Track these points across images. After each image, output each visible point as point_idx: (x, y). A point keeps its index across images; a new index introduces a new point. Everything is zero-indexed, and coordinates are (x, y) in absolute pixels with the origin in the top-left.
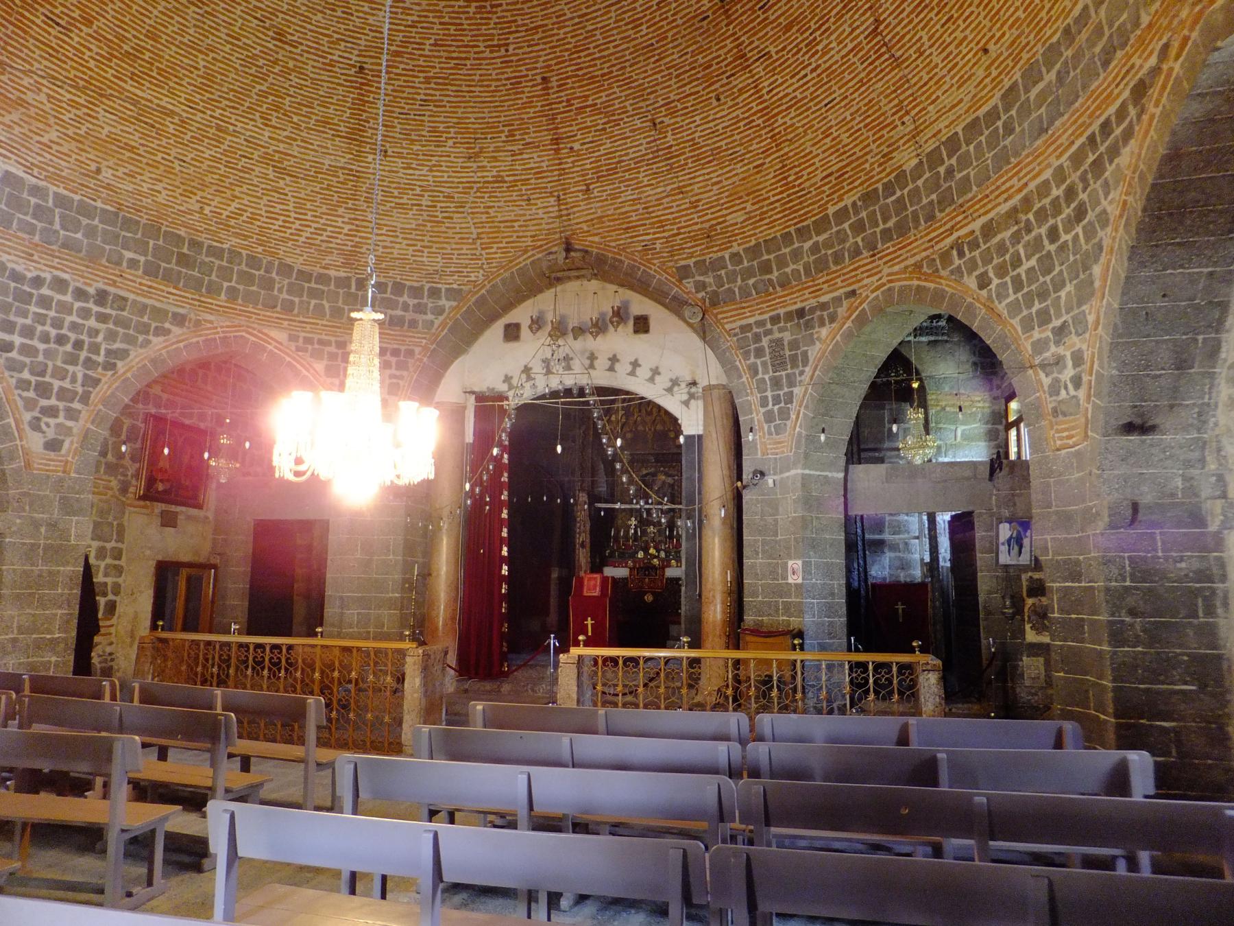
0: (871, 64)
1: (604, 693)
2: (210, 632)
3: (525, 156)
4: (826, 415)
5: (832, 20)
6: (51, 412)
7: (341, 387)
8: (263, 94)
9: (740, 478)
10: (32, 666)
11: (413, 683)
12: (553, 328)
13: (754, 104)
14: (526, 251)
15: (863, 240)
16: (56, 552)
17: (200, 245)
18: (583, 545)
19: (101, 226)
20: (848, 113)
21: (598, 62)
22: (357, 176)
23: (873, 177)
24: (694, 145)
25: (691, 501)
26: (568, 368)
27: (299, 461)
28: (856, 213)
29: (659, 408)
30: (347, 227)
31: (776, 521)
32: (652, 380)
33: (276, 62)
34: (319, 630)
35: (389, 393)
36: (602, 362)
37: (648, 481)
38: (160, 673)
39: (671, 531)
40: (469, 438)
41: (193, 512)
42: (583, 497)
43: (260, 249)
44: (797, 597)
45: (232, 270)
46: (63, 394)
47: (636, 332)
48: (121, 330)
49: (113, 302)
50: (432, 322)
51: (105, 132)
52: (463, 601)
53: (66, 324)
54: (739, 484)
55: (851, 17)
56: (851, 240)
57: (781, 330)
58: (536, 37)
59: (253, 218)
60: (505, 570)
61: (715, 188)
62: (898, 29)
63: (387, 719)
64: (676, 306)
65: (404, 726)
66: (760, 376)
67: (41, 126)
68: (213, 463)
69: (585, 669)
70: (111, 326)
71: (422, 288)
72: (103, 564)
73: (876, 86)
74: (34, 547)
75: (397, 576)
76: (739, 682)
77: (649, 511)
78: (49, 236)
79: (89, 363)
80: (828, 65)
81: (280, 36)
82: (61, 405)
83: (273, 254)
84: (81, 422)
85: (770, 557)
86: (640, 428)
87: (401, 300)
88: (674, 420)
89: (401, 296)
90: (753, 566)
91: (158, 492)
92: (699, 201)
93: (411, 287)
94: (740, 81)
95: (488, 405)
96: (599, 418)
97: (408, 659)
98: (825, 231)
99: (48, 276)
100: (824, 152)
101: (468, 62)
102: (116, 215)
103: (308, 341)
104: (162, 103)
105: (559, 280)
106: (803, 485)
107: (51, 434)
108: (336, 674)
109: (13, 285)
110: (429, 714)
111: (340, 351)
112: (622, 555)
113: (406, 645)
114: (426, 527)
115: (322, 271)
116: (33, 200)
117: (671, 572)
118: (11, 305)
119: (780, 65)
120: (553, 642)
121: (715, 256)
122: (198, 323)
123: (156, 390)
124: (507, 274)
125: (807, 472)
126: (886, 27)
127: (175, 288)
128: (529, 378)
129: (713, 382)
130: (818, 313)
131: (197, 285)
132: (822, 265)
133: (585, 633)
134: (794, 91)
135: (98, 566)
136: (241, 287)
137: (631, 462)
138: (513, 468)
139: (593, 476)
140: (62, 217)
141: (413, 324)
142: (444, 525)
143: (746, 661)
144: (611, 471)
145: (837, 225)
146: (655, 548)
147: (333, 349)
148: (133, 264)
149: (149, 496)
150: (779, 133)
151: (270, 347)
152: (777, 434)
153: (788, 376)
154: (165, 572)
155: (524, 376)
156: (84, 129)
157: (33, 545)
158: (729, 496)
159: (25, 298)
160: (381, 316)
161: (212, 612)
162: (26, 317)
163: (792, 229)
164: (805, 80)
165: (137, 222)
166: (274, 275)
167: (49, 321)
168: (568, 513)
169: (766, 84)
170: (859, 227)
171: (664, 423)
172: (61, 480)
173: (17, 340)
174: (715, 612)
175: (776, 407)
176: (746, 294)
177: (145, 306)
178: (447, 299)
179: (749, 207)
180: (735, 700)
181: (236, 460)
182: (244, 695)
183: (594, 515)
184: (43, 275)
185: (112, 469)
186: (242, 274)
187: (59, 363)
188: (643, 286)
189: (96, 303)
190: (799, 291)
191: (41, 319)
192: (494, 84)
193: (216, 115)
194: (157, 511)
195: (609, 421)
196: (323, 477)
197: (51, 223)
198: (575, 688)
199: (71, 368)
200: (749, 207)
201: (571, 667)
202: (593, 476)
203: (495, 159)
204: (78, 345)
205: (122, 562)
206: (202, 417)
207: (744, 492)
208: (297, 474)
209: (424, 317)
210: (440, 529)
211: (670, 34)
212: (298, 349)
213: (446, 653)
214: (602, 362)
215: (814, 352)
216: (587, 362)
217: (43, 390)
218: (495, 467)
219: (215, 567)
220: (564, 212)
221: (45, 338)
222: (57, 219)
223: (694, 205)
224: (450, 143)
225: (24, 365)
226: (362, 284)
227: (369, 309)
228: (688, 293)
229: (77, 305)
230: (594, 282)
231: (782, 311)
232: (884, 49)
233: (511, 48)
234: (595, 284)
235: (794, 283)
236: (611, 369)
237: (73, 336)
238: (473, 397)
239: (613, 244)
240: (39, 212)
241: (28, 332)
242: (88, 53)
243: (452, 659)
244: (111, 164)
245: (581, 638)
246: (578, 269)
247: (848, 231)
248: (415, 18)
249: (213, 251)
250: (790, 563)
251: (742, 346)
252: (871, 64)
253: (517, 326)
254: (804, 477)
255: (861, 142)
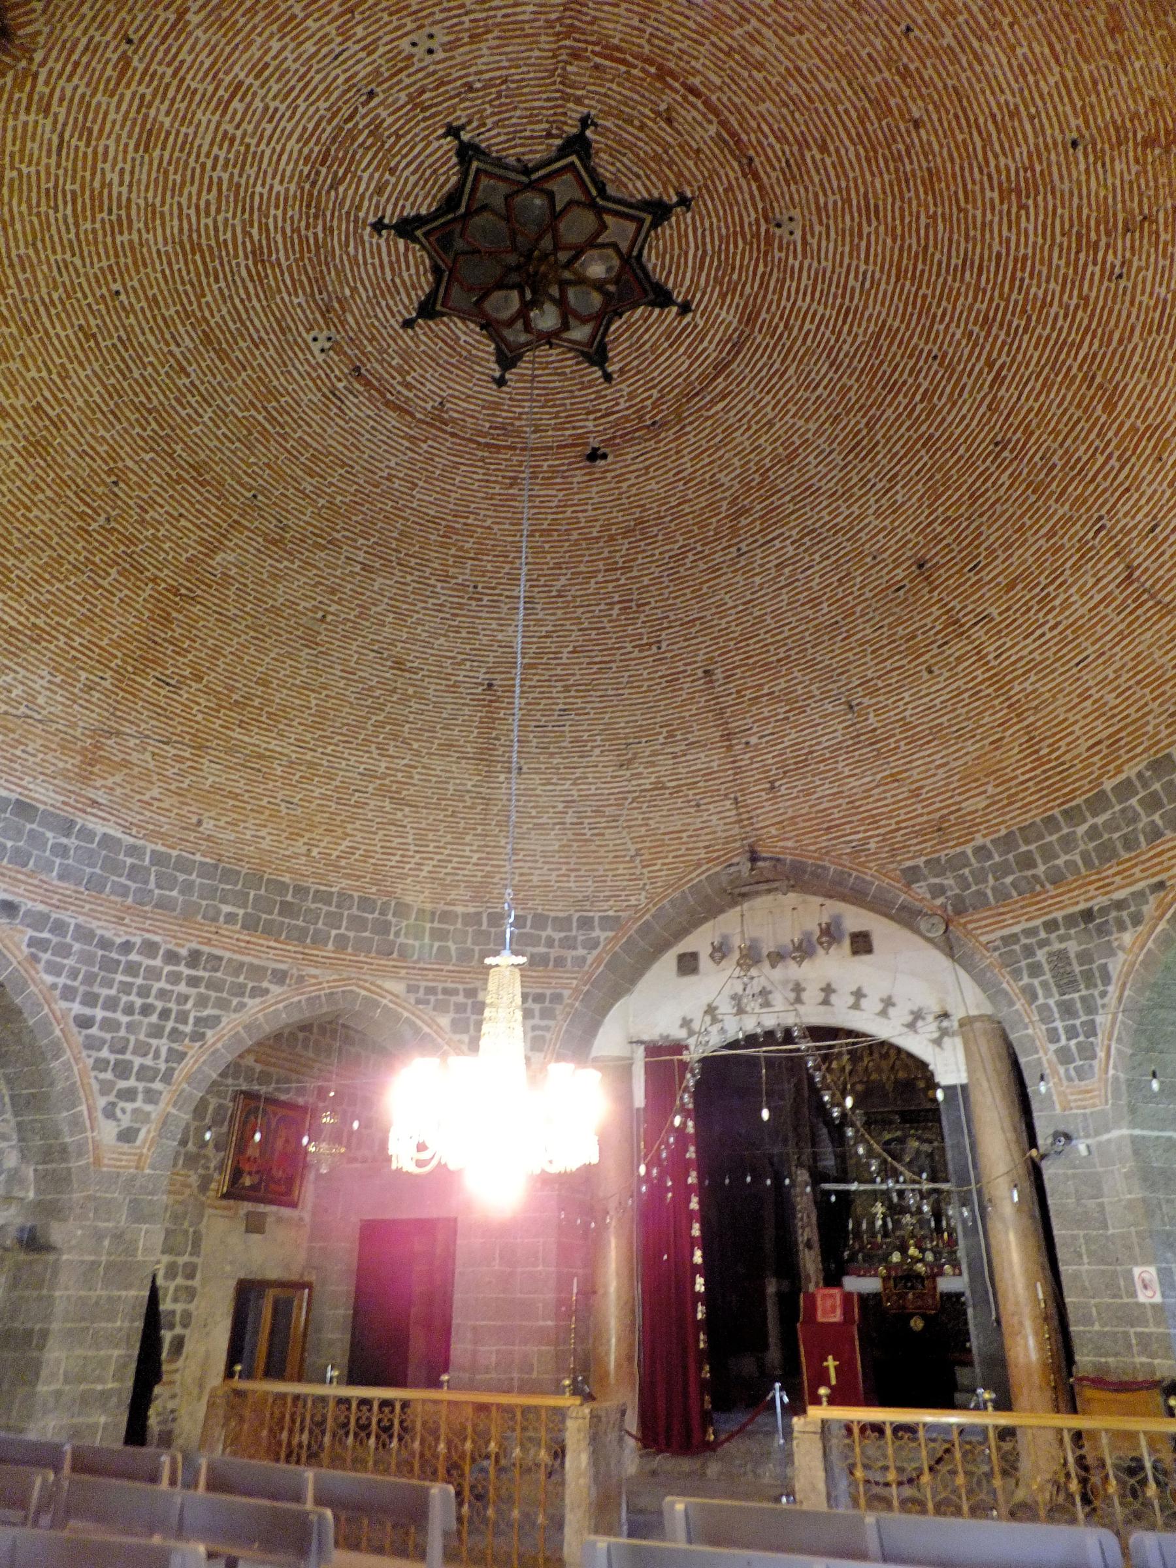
0: (1131, 613)
1: (867, 1482)
2: (300, 1379)
3: (688, 757)
4: (1152, 1049)
5: (1068, 572)
6: (129, 1095)
7: (474, 1045)
8: (380, 725)
9: (1033, 1142)
10: (76, 1432)
11: (578, 1461)
12: (742, 957)
13: (979, 672)
14: (699, 865)
15: (1162, 817)
16: (119, 1271)
17: (306, 890)
18: (809, 1245)
19: (199, 880)
20: (1109, 671)
21: (772, 648)
22: (488, 801)
23: (1160, 741)
24: (906, 725)
25: (964, 1180)
26: (767, 1004)
27: (421, 1147)
28: (1145, 785)
29: (899, 1050)
30: (477, 856)
31: (1101, 1205)
32: (883, 1013)
33: (394, 691)
34: (445, 1377)
35: (532, 1049)
36: (812, 995)
37: (894, 1150)
38: (233, 1441)
39: (938, 1221)
40: (639, 1100)
41: (285, 1212)
42: (803, 1176)
43: (374, 889)
44: (1158, 1324)
45: (342, 915)
46: (145, 1074)
47: (855, 952)
48: (213, 994)
49: (207, 961)
50: (584, 959)
51: (209, 782)
52: (643, 1330)
53: (154, 992)
54: (1034, 1152)
55: (1093, 567)
56: (1145, 820)
57: (1062, 939)
58: (693, 630)
59: (367, 855)
60: (700, 1285)
61: (941, 771)
62: (1161, 573)
63: (541, 1519)
64: (907, 917)
65: (568, 1530)
66: (1041, 1001)
67: (143, 784)
68: (312, 1149)
69: (834, 1441)
70: (202, 990)
71: (569, 919)
72: (172, 1287)
73: (1143, 637)
74: (94, 1266)
75: (550, 1296)
76: (1086, 1469)
77: (901, 1193)
78: (143, 897)
79: (175, 1035)
80: (1071, 620)
81: (399, 665)
82: (141, 1086)
83: (388, 894)
84: (162, 1105)
85: (1103, 1261)
86: (874, 1076)
87: (544, 934)
88: (923, 1066)
89: (545, 929)
90: (1076, 1276)
91: (244, 1188)
92: (922, 787)
93: (555, 919)
94: (957, 648)
95: (663, 1059)
96: (817, 1068)
97: (570, 1424)
98: (1104, 810)
99: (137, 940)
100: (1085, 717)
101: (613, 665)
102: (216, 867)
103: (431, 991)
104: (270, 747)
105: (744, 895)
106: (1136, 1152)
107: (126, 1121)
108: (468, 1445)
109: (100, 953)
110: (602, 1515)
111: (470, 1002)
112: (869, 1258)
113: (567, 1401)
114: (586, 1225)
115: (447, 908)
116: (129, 861)
117: (947, 1284)
118: (97, 975)
119: (1007, 626)
120: (779, 1396)
121: (952, 852)
122: (301, 979)
123: (250, 1061)
124: (677, 894)
125: (1137, 1132)
126: (1144, 572)
127: (276, 941)
128: (715, 1020)
129: (973, 1012)
130: (1114, 914)
131: (300, 936)
132: (1107, 853)
133: (827, 1383)
134: (1031, 653)
135: (167, 1289)
136: (352, 934)
137: (867, 1124)
138: (700, 1140)
139: (813, 1146)
140: (159, 876)
141: (560, 962)
142: (611, 1221)
143: (1093, 1434)
144: (838, 1138)
145: (1120, 802)
146: (917, 1246)
147: (460, 999)
148: (231, 918)
149: (234, 1193)
150: (1018, 701)
151: (385, 1001)
152: (1081, 1079)
153: (1083, 998)
154: (247, 1293)
155: (708, 1019)
156: (187, 781)
157: (93, 1263)
158: (1022, 1170)
159: (110, 966)
160: (522, 960)
161: (303, 1350)
162: (111, 987)
163: (1056, 812)
164: (1043, 640)
165: (238, 873)
166: (390, 917)
167: (135, 990)
168: (782, 1201)
169: (992, 648)
170: (1153, 803)
171: (906, 1067)
172: (133, 1178)
173: (99, 1013)
174: (1027, 1348)
175: (1073, 1042)
176: (1002, 895)
177: (242, 965)
178: (603, 929)
179: (991, 790)
180: (1086, 1500)
181: (340, 1144)
182: (343, 1478)
183: (821, 1199)
184: (133, 939)
185: (192, 1160)
186: (352, 918)
187: (142, 1037)
188: (858, 896)
189: (188, 965)
190: (1080, 887)
191: (126, 988)
192: (646, 684)
193: (328, 751)
194: (242, 1212)
195: (829, 1070)
196: (451, 1167)
197: (146, 882)
198: (821, 1474)
199: (154, 1042)
200: (991, 790)
201: (814, 1435)
202: (814, 1145)
203: (652, 764)
204: (165, 1014)
205: (196, 1283)
206: (301, 1091)
207: (1044, 1165)
208: (420, 1164)
209: (574, 953)
210: (607, 1227)
211: (859, 608)
212: (418, 1002)
213: (623, 1413)
214: (812, 995)
215: (1116, 965)
216: (792, 996)
217: (122, 1070)
218: (676, 1140)
219: (309, 1286)
220: (745, 816)
221: (129, 1010)
222: (153, 878)
223: (915, 793)
224: (597, 751)
225: (104, 1042)
226: (497, 919)
227: (507, 952)
228: (922, 900)
229: (167, 969)
230: (791, 895)
231: (1059, 915)
232: (1145, 596)
233: (664, 644)
234: (792, 898)
235: (1071, 878)
236: (826, 1002)
237: (159, 1005)
238: (642, 1048)
239: (813, 848)
240: (135, 872)
241: (111, 1004)
242: (197, 708)
243: (632, 1423)
244: (212, 814)
245: (823, 1391)
246: (767, 881)
247: (1139, 809)
248: (549, 628)
249: (320, 897)
250: (1137, 1271)
251: (1008, 961)
252: (1131, 613)
253: (694, 956)
254: (1134, 1140)
255: (1136, 701)
